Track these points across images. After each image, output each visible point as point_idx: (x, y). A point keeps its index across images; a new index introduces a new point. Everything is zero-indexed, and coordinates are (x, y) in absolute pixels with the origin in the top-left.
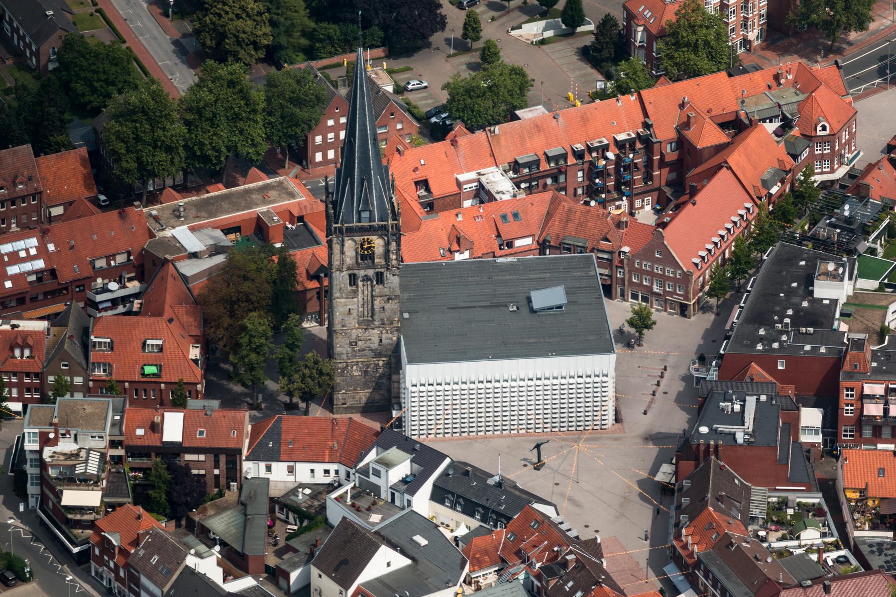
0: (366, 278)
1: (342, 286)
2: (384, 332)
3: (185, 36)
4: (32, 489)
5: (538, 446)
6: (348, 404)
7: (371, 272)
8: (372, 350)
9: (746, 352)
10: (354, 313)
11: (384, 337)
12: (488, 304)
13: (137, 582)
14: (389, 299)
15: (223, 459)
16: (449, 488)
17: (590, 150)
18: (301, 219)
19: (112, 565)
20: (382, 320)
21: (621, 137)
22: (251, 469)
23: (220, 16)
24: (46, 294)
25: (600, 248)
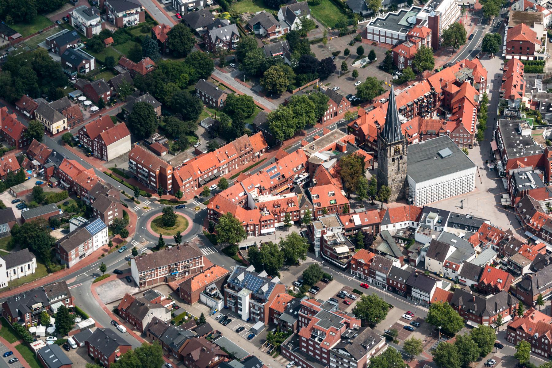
3: (253, 86)
4: (317, 249)
5: (462, 201)
9: (514, 158)
13: (374, 274)
15: (375, 227)
16: (454, 222)
17: (419, 100)
18: (348, 142)
19: (362, 269)
21: (426, 94)
23: (272, 79)
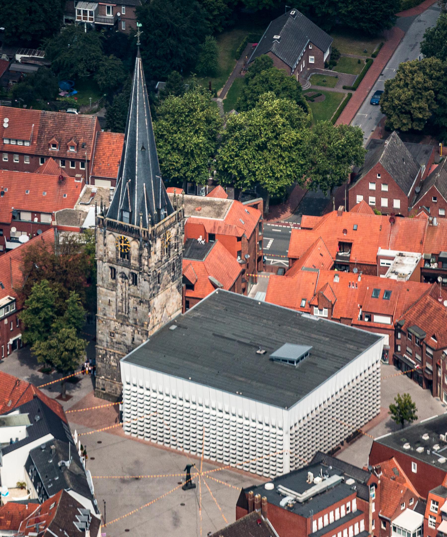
0: (124, 276)
1: (104, 276)
2: (136, 331)
6: (107, 391)
7: (127, 271)
8: (126, 346)
11: (136, 336)
12: (248, 342)
20: (135, 320)
25: (428, 343)
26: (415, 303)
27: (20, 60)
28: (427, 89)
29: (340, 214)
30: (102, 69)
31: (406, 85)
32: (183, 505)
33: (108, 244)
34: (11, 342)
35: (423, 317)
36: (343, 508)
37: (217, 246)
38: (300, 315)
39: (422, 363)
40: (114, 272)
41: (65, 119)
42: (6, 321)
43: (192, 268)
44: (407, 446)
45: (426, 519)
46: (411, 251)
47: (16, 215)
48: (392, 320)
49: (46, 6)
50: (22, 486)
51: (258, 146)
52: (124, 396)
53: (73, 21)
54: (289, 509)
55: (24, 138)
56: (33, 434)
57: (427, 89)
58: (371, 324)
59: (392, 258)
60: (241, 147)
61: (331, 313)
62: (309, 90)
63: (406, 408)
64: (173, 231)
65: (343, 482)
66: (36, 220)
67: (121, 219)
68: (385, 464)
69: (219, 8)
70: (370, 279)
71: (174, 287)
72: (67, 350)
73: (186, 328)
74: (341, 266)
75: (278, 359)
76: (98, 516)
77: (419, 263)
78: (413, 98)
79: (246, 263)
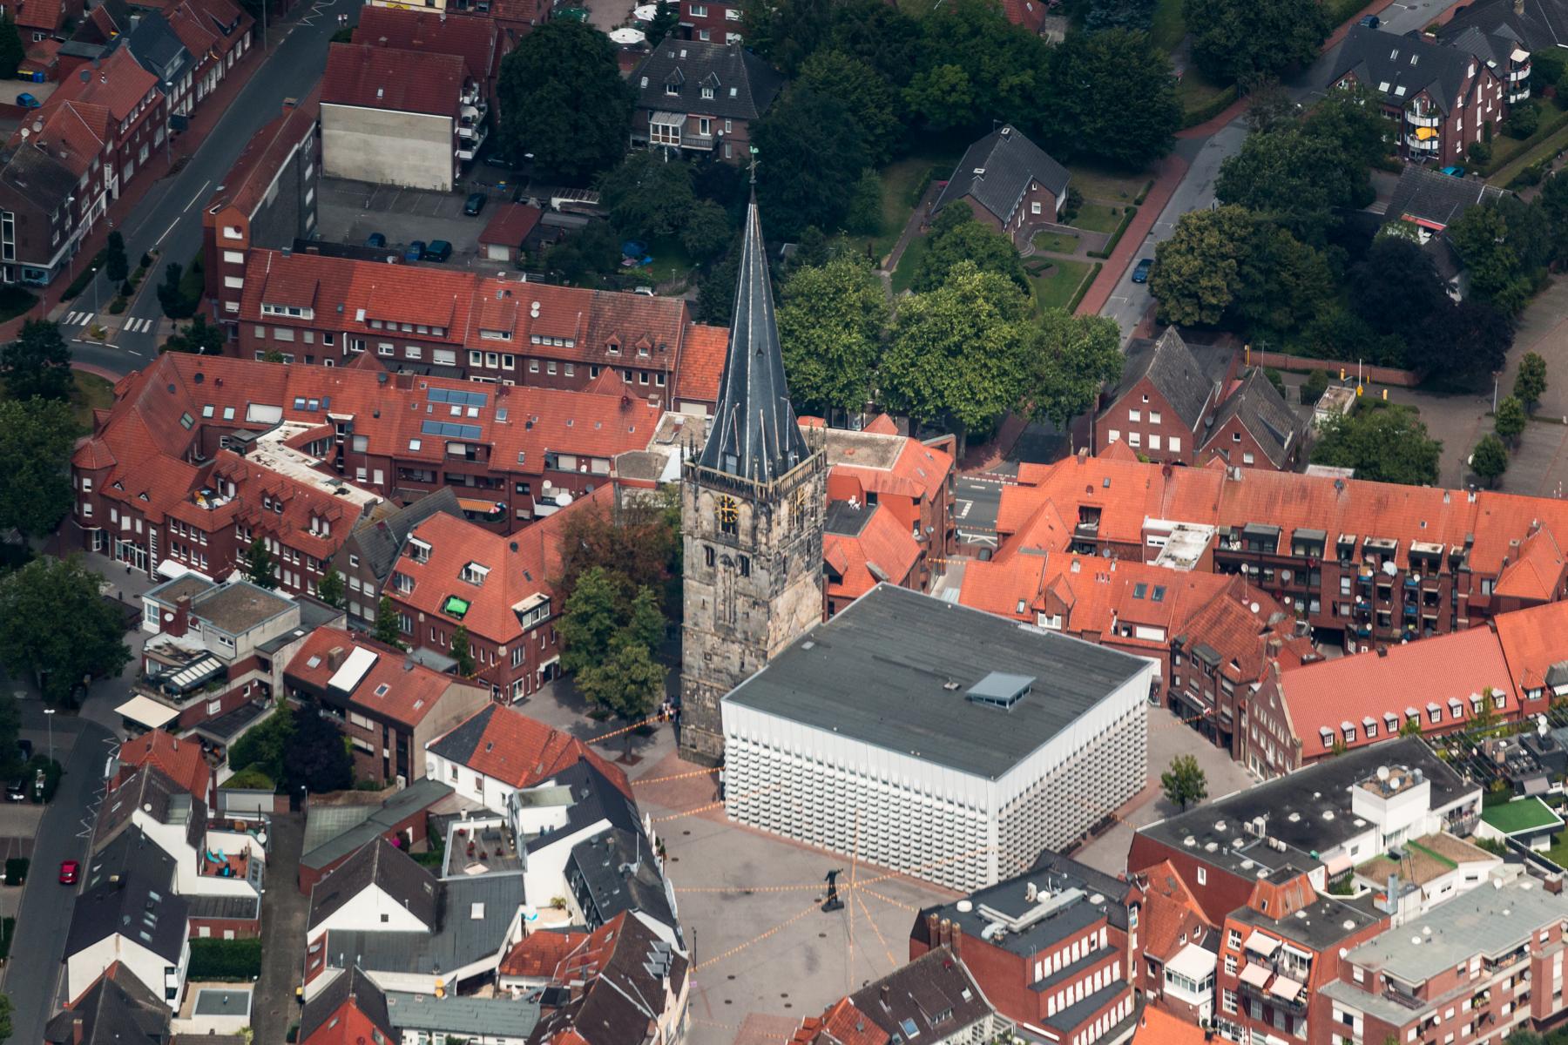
6: (699, 749)
7: (732, 553)
10: (710, 608)
11: (747, 659)
12: (930, 669)
14: (755, 603)
15: (393, 735)
20: (745, 633)
21: (1418, 547)
22: (436, 768)
24: (478, 479)
26: (1205, 607)
27: (1321, 304)
28: (1224, 257)
29: (1082, 461)
30: (693, 223)
31: (1191, 250)
32: (822, 935)
33: (703, 508)
34: (542, 668)
35: (1218, 630)
36: (1085, 941)
37: (880, 513)
38: (1016, 626)
39: (1215, 705)
40: (710, 552)
41: (632, 304)
42: (534, 634)
43: (839, 549)
44: (1190, 842)
45: (1220, 960)
46: (1197, 521)
47: (551, 461)
48: (1166, 635)
49: (601, 118)
50: (559, 905)
51: (948, 349)
52: (728, 758)
53: (645, 144)
54: (996, 943)
55: (565, 335)
56: (578, 819)
57: (1224, 257)
58: (1132, 641)
59: (1167, 534)
60: (920, 351)
61: (1066, 623)
62: (1032, 258)
63: (1189, 778)
64: (808, 488)
65: (1085, 899)
66: (584, 469)
67: (724, 469)
68: (1155, 870)
69: (884, 123)
70: (1131, 567)
71: (810, 579)
72: (633, 682)
73: (828, 646)
74: (1084, 546)
75: (980, 699)
76: (684, 954)
77: (1211, 541)
78: (1201, 271)
79: (928, 541)
